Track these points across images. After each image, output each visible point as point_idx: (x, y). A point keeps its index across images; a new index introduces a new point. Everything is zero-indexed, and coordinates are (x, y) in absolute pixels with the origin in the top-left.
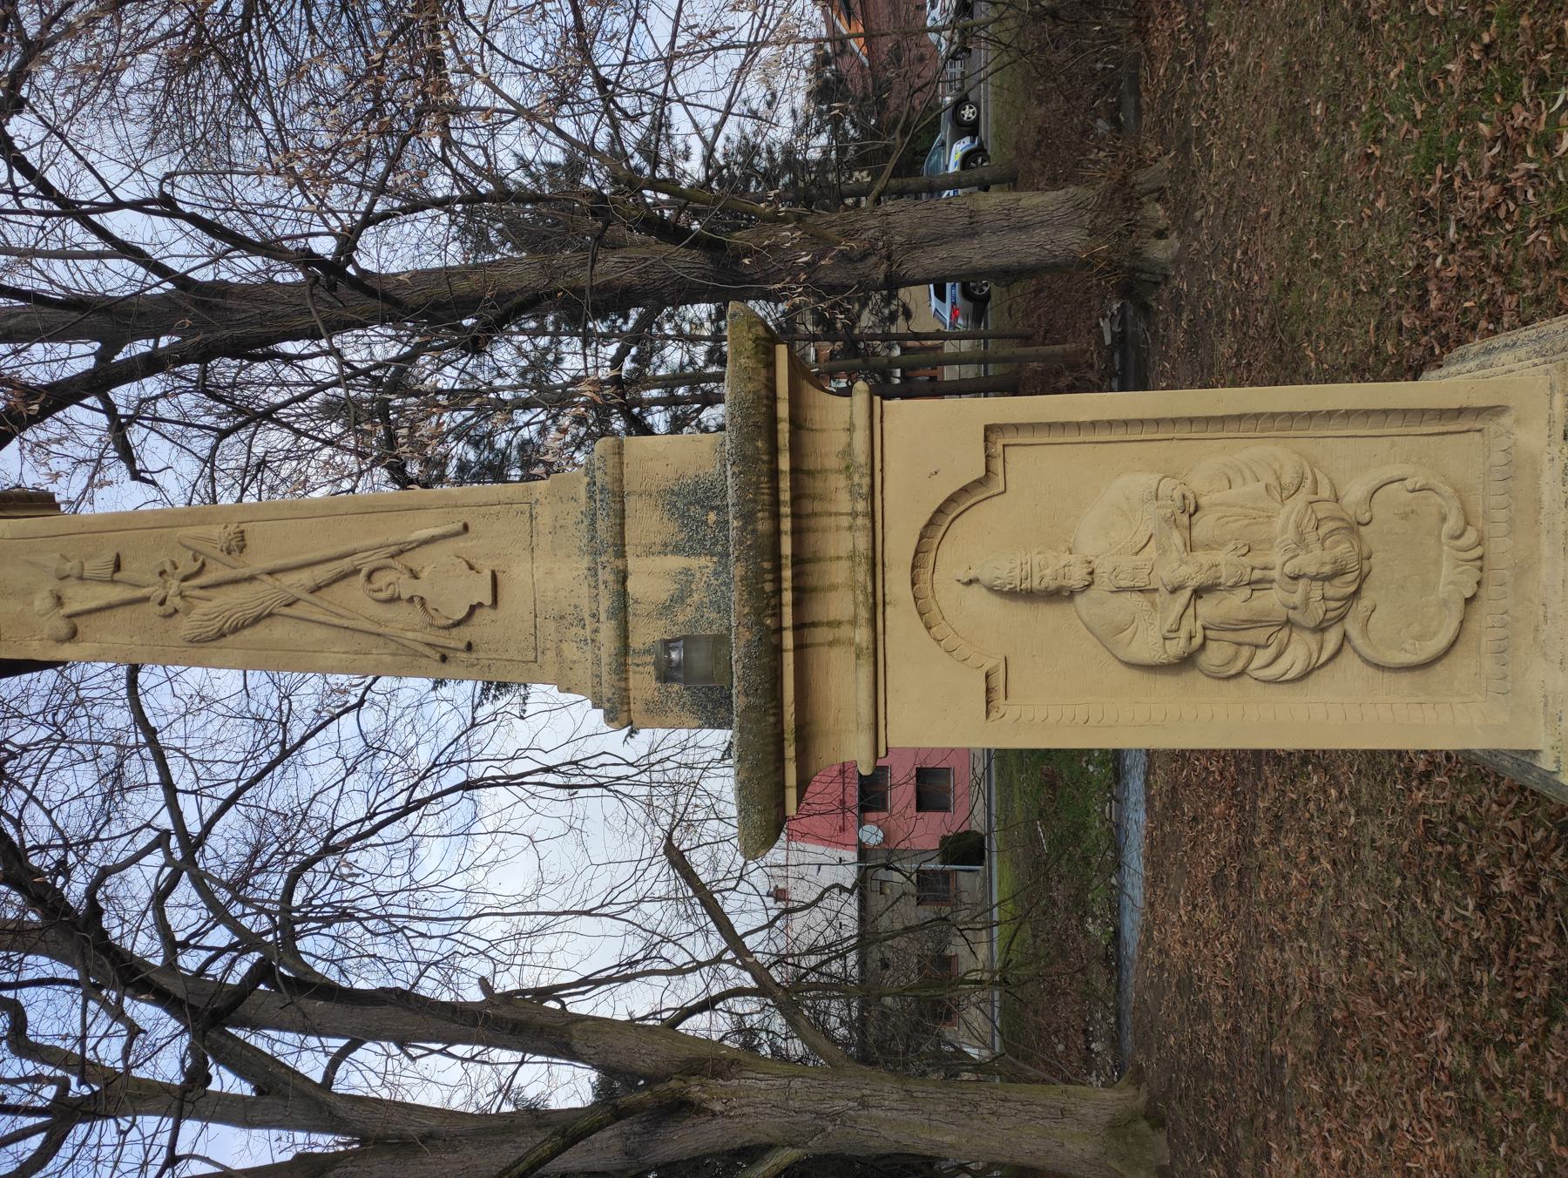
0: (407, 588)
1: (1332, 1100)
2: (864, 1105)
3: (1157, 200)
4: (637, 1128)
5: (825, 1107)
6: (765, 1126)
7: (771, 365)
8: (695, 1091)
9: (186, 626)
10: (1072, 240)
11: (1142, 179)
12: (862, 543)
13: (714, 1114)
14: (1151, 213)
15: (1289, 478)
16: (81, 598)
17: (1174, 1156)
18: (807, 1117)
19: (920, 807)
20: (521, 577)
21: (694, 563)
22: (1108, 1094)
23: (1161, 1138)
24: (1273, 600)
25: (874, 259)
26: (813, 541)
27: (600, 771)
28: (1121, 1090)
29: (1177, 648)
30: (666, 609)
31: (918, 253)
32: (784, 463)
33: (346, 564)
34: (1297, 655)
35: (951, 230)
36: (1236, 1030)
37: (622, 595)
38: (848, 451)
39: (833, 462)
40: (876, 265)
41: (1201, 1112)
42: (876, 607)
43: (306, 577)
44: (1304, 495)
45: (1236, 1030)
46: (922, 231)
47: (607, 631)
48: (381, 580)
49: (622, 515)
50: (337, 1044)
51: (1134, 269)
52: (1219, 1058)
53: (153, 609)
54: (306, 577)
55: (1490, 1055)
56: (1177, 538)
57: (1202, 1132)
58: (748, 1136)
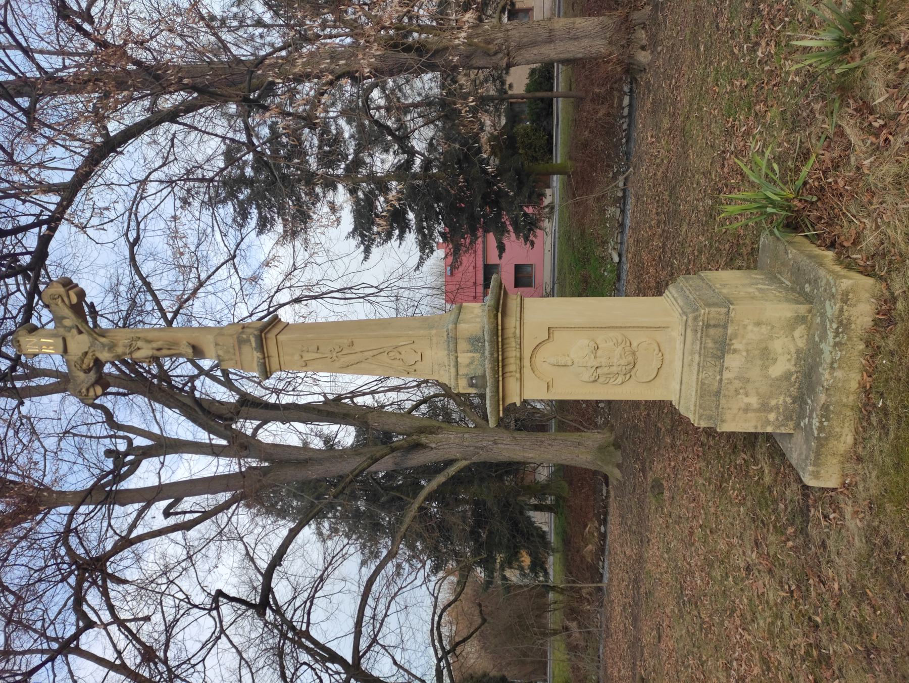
0: (398, 356)
1: (673, 446)
2: (495, 443)
3: (643, 28)
4: (399, 454)
5: (479, 444)
6: (454, 453)
7: (497, 319)
8: (423, 439)
9: (337, 364)
10: (599, 46)
11: (635, 17)
12: (518, 355)
13: (432, 448)
14: (639, 36)
15: (620, 341)
16: (307, 356)
17: (623, 459)
18: (472, 448)
19: (516, 287)
20: (428, 354)
21: (475, 355)
22: (599, 436)
23: (619, 453)
24: (614, 369)
25: (500, 55)
26: (506, 354)
27: (361, 291)
28: (604, 434)
29: (592, 379)
30: (468, 365)
31: (523, 51)
32: (500, 339)
33: (382, 350)
34: (620, 380)
35: (540, 39)
36: (648, 415)
37: (457, 362)
38: (515, 333)
39: (511, 335)
40: (502, 59)
41: (634, 443)
42: (521, 368)
43: (371, 353)
44: (623, 345)
45: (648, 415)
46: (525, 40)
47: (453, 370)
48: (391, 354)
49: (456, 343)
50: (258, 422)
51: (631, 64)
52: (642, 424)
53: (329, 360)
54: (371, 353)
55: (711, 439)
56: (593, 356)
57: (634, 451)
58: (446, 456)
